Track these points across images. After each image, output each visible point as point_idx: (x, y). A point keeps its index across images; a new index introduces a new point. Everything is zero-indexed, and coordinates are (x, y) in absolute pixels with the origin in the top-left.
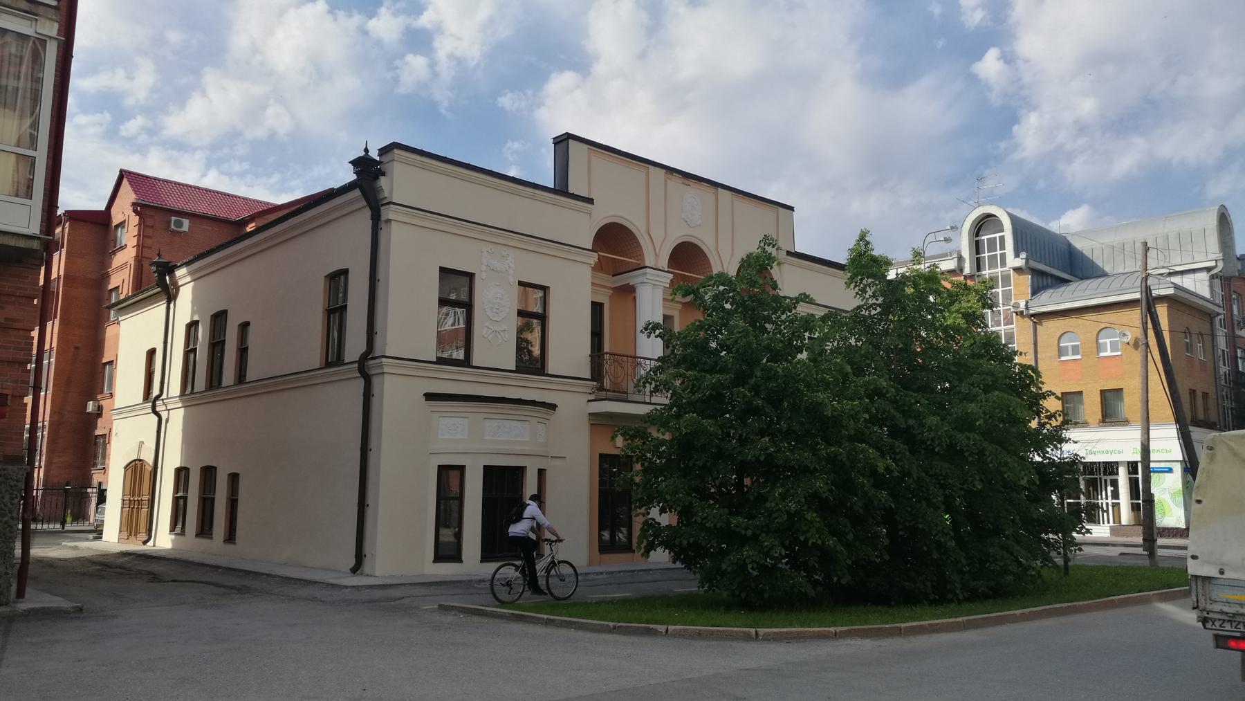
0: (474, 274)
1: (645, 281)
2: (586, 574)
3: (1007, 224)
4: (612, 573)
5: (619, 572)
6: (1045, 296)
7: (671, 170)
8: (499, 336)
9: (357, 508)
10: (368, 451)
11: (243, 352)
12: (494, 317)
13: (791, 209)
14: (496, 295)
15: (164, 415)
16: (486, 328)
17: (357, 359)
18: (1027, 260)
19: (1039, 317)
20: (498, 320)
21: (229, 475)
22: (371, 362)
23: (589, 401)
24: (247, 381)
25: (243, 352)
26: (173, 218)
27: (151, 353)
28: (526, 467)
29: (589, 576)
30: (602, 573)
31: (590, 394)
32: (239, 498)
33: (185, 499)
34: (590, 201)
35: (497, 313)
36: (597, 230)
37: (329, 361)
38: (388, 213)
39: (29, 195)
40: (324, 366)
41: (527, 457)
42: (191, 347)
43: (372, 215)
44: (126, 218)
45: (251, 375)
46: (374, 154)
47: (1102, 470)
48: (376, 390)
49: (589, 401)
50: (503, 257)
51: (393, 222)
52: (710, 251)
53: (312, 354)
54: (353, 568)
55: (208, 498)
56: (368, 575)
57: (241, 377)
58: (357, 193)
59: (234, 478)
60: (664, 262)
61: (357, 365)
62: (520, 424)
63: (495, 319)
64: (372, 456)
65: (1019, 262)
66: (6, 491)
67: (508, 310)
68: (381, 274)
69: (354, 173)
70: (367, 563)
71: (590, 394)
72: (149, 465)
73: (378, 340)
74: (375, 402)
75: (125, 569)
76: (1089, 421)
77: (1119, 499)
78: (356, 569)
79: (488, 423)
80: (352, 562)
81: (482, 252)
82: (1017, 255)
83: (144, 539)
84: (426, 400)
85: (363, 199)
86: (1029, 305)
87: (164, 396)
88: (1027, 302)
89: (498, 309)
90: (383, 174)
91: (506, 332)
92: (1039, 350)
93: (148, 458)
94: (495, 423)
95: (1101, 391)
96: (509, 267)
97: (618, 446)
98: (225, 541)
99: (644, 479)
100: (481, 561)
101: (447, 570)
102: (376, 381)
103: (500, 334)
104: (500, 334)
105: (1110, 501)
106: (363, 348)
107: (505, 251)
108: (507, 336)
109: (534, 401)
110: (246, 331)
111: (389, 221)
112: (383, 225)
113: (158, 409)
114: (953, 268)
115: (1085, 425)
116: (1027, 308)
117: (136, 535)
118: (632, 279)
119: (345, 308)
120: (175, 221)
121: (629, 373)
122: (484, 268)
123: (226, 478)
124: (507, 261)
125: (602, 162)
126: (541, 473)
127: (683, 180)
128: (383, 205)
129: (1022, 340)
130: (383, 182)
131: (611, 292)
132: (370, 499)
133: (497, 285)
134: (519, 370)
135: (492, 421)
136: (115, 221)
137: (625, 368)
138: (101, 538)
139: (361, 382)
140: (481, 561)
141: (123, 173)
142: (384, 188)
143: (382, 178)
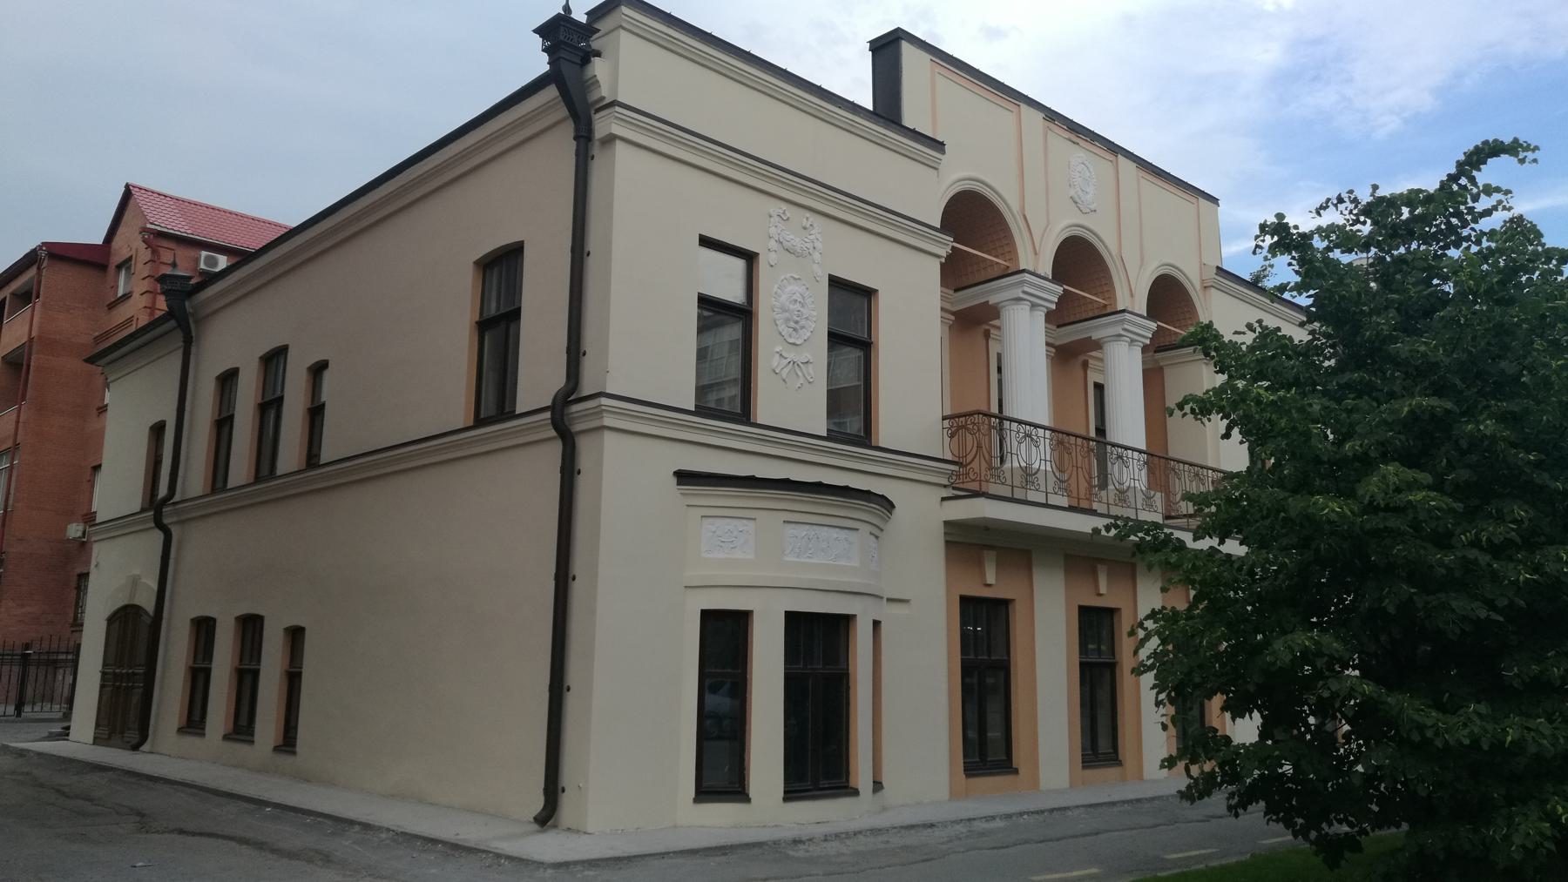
0: (758, 254)
1: (1022, 296)
2: (969, 820)
4: (1008, 816)
5: (1021, 814)
7: (1052, 116)
8: (800, 374)
9: (547, 694)
10: (570, 580)
11: (316, 413)
12: (790, 336)
13: (1214, 200)
14: (794, 297)
15: (175, 531)
16: (777, 356)
17: (549, 403)
20: (798, 343)
21: (287, 630)
22: (575, 408)
23: (943, 499)
24: (322, 462)
25: (316, 413)
26: (204, 253)
27: (158, 430)
28: (855, 616)
29: (975, 823)
30: (993, 818)
31: (945, 486)
32: (303, 670)
34: (939, 146)
35: (795, 329)
36: (946, 201)
37: (482, 416)
38: (604, 125)
40: (471, 424)
41: (858, 598)
42: (225, 415)
43: (577, 129)
44: (133, 252)
45: (327, 455)
46: (580, 16)
48: (584, 461)
49: (943, 499)
50: (805, 228)
51: (619, 145)
52: (1112, 258)
53: (455, 406)
54: (540, 814)
55: (249, 671)
56: (569, 829)
57: (312, 458)
58: (551, 92)
59: (296, 635)
60: (1046, 268)
61: (548, 415)
62: (843, 534)
63: (791, 341)
64: (577, 590)
67: (809, 334)
68: (593, 242)
69: (543, 50)
70: (567, 803)
71: (945, 486)
72: (146, 613)
73: (588, 367)
74: (583, 484)
75: (91, 800)
78: (547, 817)
79: (791, 530)
80: (537, 803)
81: (771, 216)
83: (134, 741)
84: (678, 484)
85: (563, 104)
87: (177, 498)
89: (797, 322)
90: (598, 54)
91: (810, 366)
93: (148, 603)
94: (803, 531)
96: (814, 248)
97: (988, 582)
98: (277, 749)
100: (786, 799)
101: (721, 820)
102: (584, 445)
103: (801, 369)
104: (801, 369)
106: (559, 380)
107: (807, 219)
108: (811, 372)
109: (869, 491)
110: (321, 379)
111: (611, 139)
112: (596, 150)
113: (166, 521)
117: (122, 733)
118: (995, 294)
119: (515, 314)
120: (207, 258)
121: (1079, 465)
122: (773, 244)
123: (281, 634)
124: (811, 237)
126: (876, 624)
127: (1067, 135)
128: (598, 111)
130: (599, 67)
131: (953, 318)
132: (573, 676)
133: (795, 279)
134: (831, 437)
135: (797, 526)
136: (116, 259)
137: (1074, 454)
138: (68, 735)
139: (556, 449)
140: (786, 799)
141: (131, 188)
142: (599, 78)
143: (596, 60)
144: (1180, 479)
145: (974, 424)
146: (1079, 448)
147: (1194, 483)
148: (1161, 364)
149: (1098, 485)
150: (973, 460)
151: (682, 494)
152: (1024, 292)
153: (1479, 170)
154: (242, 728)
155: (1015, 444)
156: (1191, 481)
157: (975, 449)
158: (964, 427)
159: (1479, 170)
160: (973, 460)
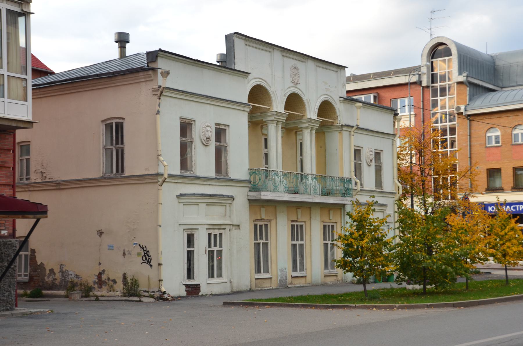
1: (274, 119)
3: (454, 51)
6: (478, 102)
18: (467, 76)
19: (471, 117)
33: (220, 252)
39: (26, 100)
47: (266, 169)
65: (462, 78)
66: (12, 252)
76: (505, 187)
77: (300, 241)
82: (460, 73)
86: (468, 108)
88: (466, 106)
92: (473, 139)
95: (514, 168)
99: (521, 245)
105: (331, 242)
114: (415, 81)
115: (502, 191)
116: (466, 110)
121: (292, 181)
125: (253, 52)
129: (461, 133)
137: (290, 178)
144: (335, 183)
145: (258, 172)
146: (291, 176)
147: (331, 183)
148: (324, 131)
149: (14, 197)
150: (278, 185)
151: (184, 205)
152: (275, 118)
153: (341, 268)
154: (215, 236)
155: (329, 183)
156: (338, 183)
157: (259, 180)
158: (255, 173)
159: (341, 268)
160: (278, 185)
